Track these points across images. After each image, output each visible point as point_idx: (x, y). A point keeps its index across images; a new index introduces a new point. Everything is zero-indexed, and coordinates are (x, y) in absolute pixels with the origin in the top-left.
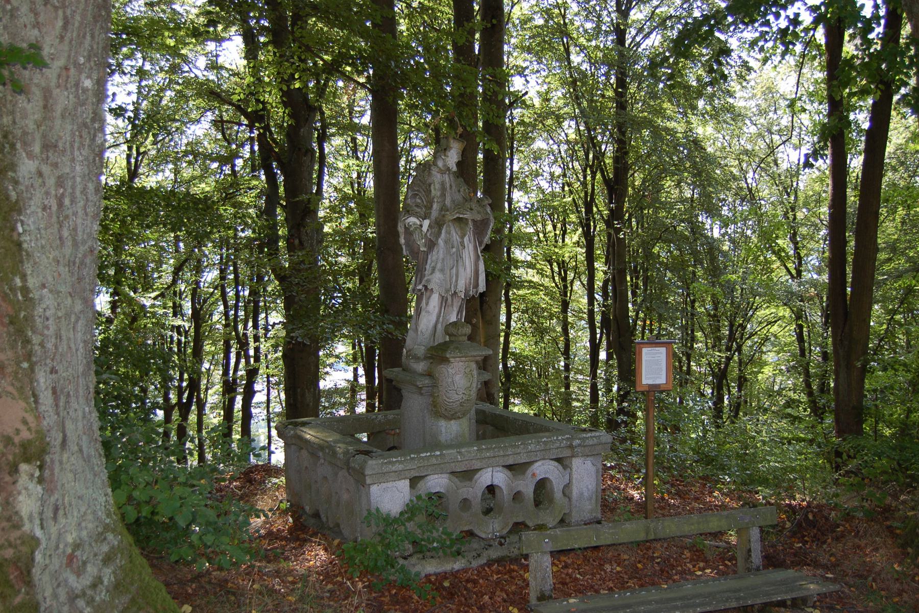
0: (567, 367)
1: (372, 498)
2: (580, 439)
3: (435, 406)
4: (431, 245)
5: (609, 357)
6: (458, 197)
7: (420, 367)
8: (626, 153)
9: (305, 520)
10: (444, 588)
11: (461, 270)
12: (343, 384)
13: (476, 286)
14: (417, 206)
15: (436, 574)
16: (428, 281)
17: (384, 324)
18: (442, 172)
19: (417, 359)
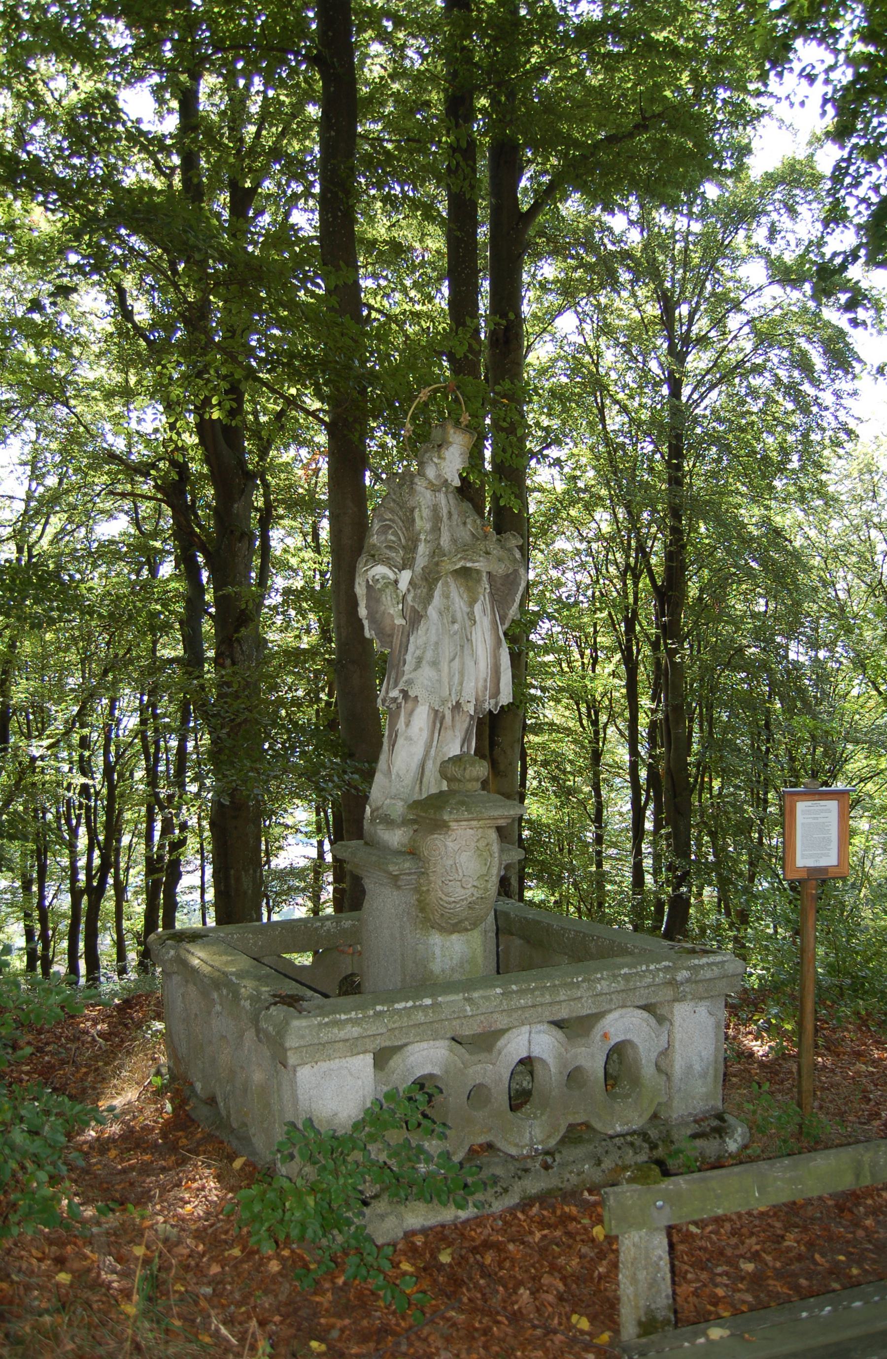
0: (599, 840)
1: (300, 1092)
2: (688, 968)
3: (422, 910)
4: (415, 619)
5: (658, 826)
6: (464, 534)
7: (395, 838)
8: (683, 547)
9: (194, 1108)
10: (441, 1267)
11: (469, 663)
12: (302, 863)
13: (496, 693)
14: (389, 548)
15: (424, 1231)
16: (410, 682)
17: (345, 772)
18: (434, 489)
19: (388, 822)
